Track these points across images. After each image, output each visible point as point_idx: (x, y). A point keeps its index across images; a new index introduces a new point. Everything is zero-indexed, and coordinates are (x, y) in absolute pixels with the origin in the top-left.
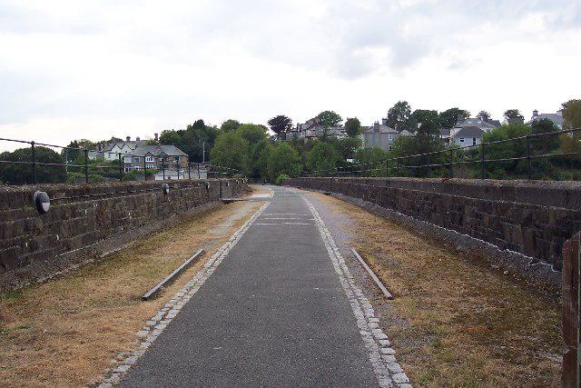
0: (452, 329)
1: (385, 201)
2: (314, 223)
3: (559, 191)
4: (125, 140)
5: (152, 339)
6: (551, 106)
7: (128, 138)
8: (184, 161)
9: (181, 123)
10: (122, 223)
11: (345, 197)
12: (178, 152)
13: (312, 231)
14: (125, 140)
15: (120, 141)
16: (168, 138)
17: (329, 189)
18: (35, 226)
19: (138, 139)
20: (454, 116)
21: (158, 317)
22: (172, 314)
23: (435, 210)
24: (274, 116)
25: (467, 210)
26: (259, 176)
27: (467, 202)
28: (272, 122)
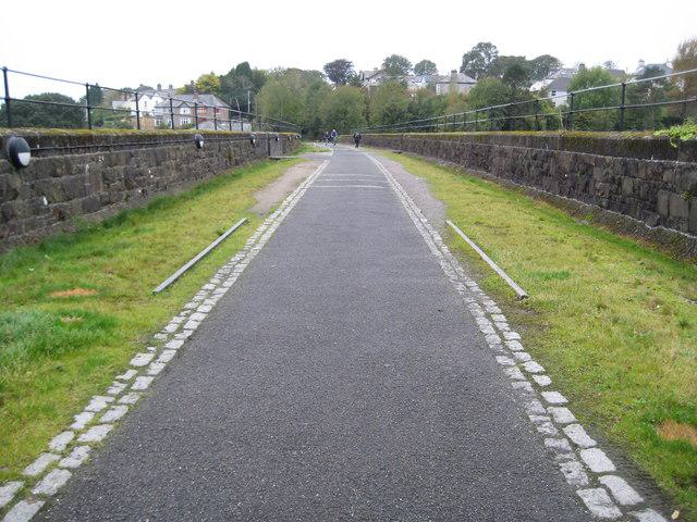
0: (54, 218)
1: (475, 160)
2: (386, 185)
3: (16, 127)
4: (155, 88)
5: (157, 368)
6: (664, 53)
7: (159, 86)
8: (223, 114)
9: (223, 68)
10: (140, 184)
11: (419, 157)
12: (218, 104)
13: (387, 195)
14: (155, 88)
15: (150, 88)
16: (207, 86)
17: (401, 147)
18: (9, 186)
19: (171, 87)
20: (546, 65)
21: (171, 328)
22: (192, 325)
23: (546, 173)
24: (332, 60)
25: (597, 173)
26: (315, 131)
27: (599, 163)
28: (329, 67)
